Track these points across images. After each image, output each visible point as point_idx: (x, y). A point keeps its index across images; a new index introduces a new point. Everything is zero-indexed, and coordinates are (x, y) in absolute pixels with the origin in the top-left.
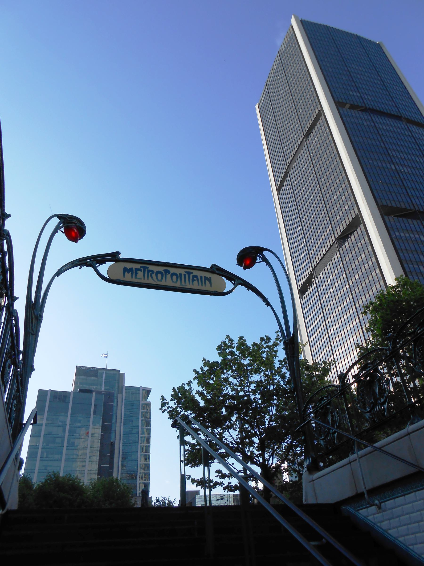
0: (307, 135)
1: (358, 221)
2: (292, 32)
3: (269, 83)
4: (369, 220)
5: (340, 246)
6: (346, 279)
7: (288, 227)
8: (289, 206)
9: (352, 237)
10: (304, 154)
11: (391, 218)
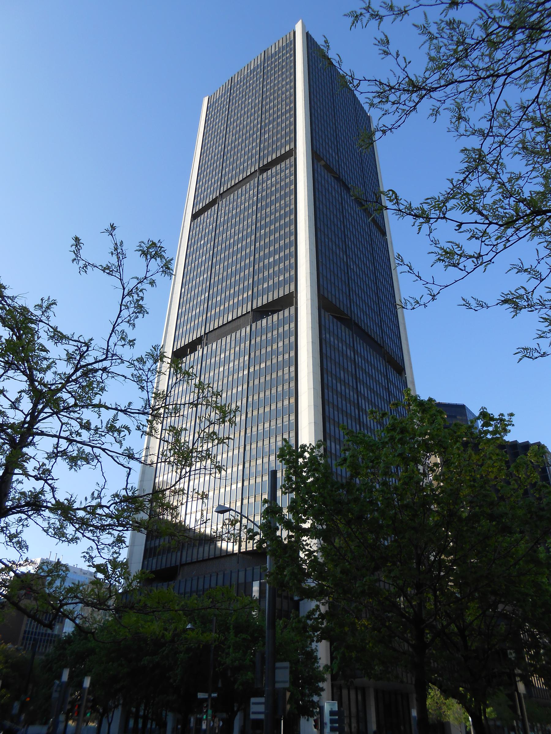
0: (264, 169)
1: (289, 300)
2: (292, 38)
3: (236, 81)
4: (305, 304)
5: (255, 320)
6: (247, 363)
7: (189, 267)
8: (202, 242)
9: (275, 316)
10: (250, 189)
11: (327, 314)
